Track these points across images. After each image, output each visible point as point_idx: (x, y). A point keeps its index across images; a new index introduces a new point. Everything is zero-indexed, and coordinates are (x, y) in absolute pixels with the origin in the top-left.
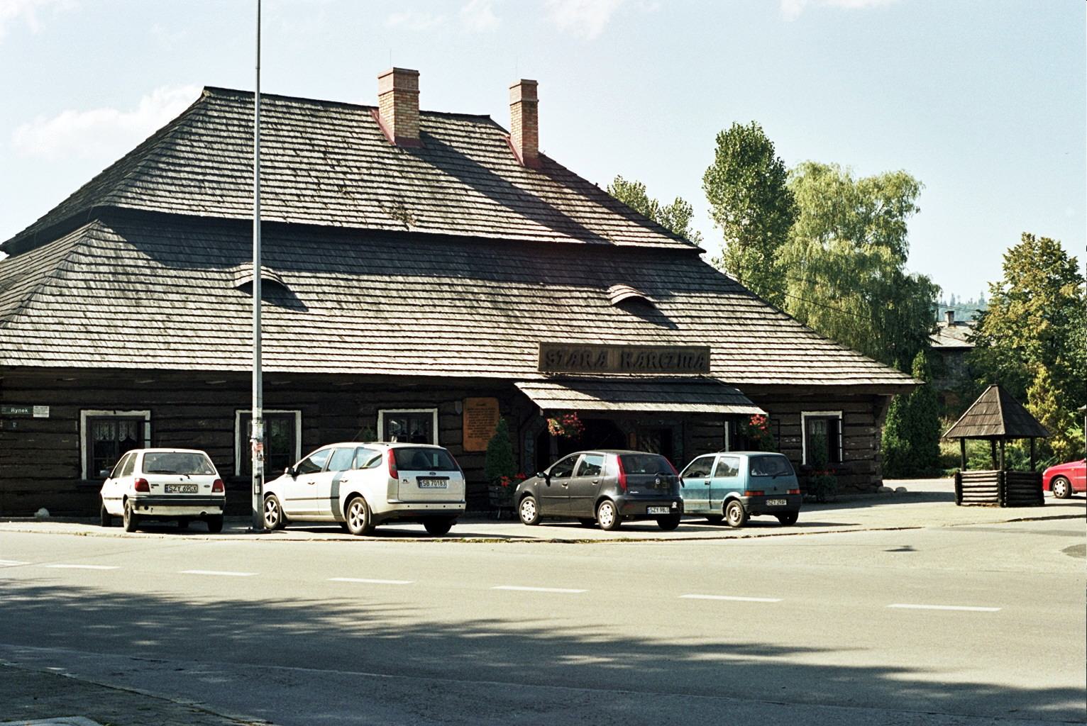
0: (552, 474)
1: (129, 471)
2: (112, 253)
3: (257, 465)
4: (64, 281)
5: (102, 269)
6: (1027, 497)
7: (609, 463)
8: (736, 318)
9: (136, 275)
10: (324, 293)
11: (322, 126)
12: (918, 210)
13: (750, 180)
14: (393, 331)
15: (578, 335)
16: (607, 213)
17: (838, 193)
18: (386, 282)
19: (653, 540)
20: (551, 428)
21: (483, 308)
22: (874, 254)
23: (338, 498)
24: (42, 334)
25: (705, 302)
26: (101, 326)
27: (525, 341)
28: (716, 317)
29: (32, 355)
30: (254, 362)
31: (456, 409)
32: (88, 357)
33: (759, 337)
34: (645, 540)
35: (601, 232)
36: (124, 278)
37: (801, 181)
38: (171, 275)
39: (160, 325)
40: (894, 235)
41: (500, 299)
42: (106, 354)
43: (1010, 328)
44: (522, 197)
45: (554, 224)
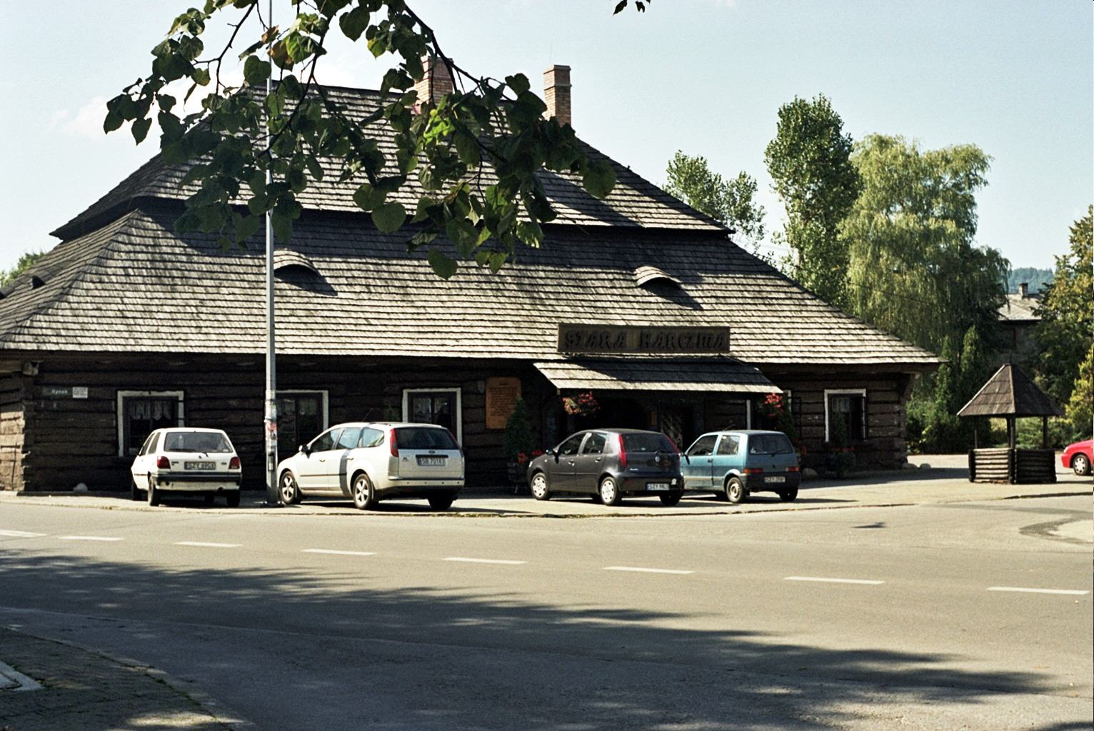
0: (561, 452)
1: (153, 450)
2: (151, 241)
3: (271, 444)
4: (103, 269)
5: (140, 256)
6: (1038, 474)
7: (613, 440)
8: (762, 298)
9: (172, 262)
10: (353, 277)
11: (359, 114)
12: (986, 183)
13: (811, 154)
14: (418, 314)
15: (601, 316)
16: (637, 196)
17: (905, 166)
18: (415, 266)
19: (644, 515)
20: (567, 407)
21: (508, 290)
22: (939, 228)
23: (345, 474)
24: (81, 320)
25: (729, 284)
26: (137, 311)
27: (548, 323)
28: (742, 298)
29: (70, 340)
30: (267, 345)
31: (479, 389)
32: (123, 342)
33: (784, 317)
34: (635, 515)
35: (630, 214)
36: (161, 265)
37: (867, 154)
38: (206, 262)
39: (194, 310)
40: (962, 211)
41: (526, 281)
42: (141, 339)
43: (1075, 301)
44: (554, 181)
45: (582, 207)
